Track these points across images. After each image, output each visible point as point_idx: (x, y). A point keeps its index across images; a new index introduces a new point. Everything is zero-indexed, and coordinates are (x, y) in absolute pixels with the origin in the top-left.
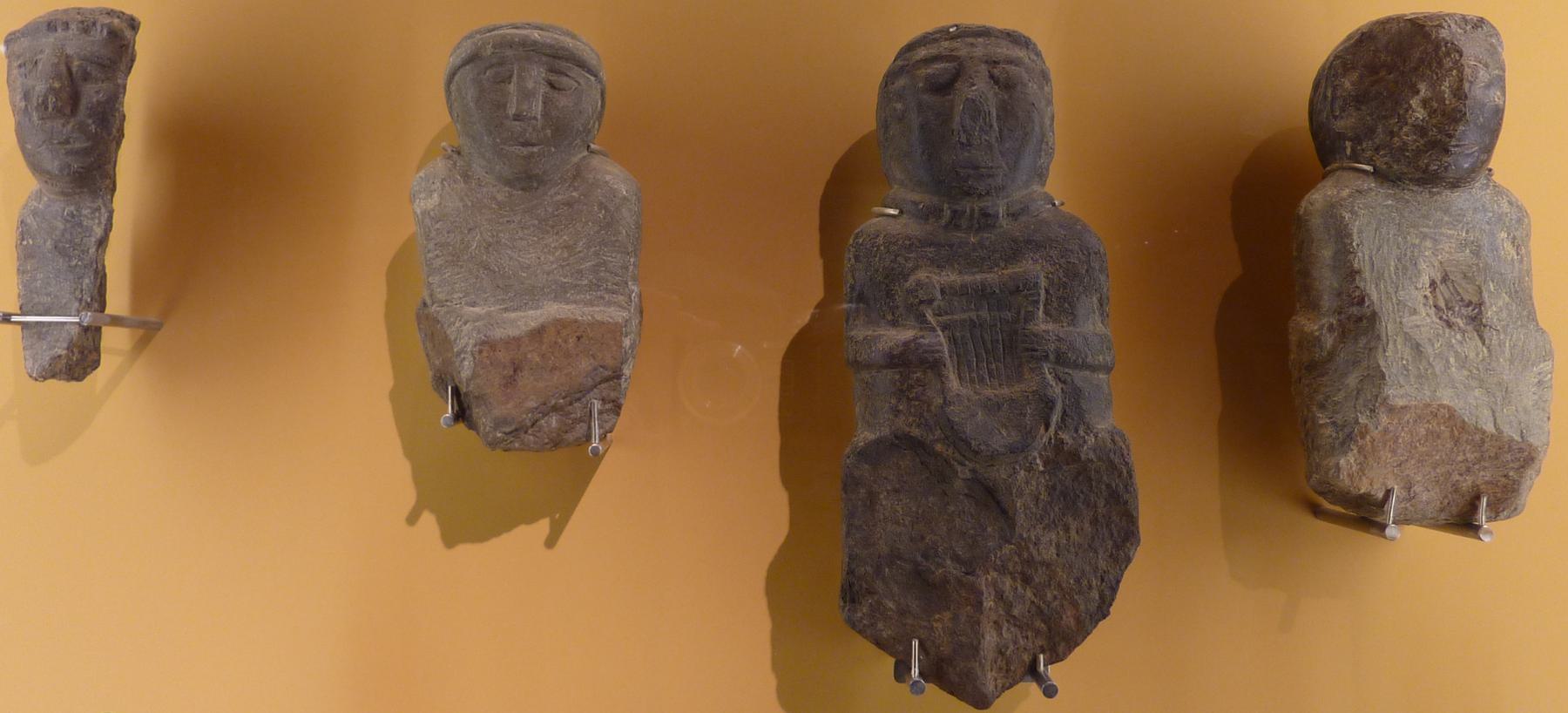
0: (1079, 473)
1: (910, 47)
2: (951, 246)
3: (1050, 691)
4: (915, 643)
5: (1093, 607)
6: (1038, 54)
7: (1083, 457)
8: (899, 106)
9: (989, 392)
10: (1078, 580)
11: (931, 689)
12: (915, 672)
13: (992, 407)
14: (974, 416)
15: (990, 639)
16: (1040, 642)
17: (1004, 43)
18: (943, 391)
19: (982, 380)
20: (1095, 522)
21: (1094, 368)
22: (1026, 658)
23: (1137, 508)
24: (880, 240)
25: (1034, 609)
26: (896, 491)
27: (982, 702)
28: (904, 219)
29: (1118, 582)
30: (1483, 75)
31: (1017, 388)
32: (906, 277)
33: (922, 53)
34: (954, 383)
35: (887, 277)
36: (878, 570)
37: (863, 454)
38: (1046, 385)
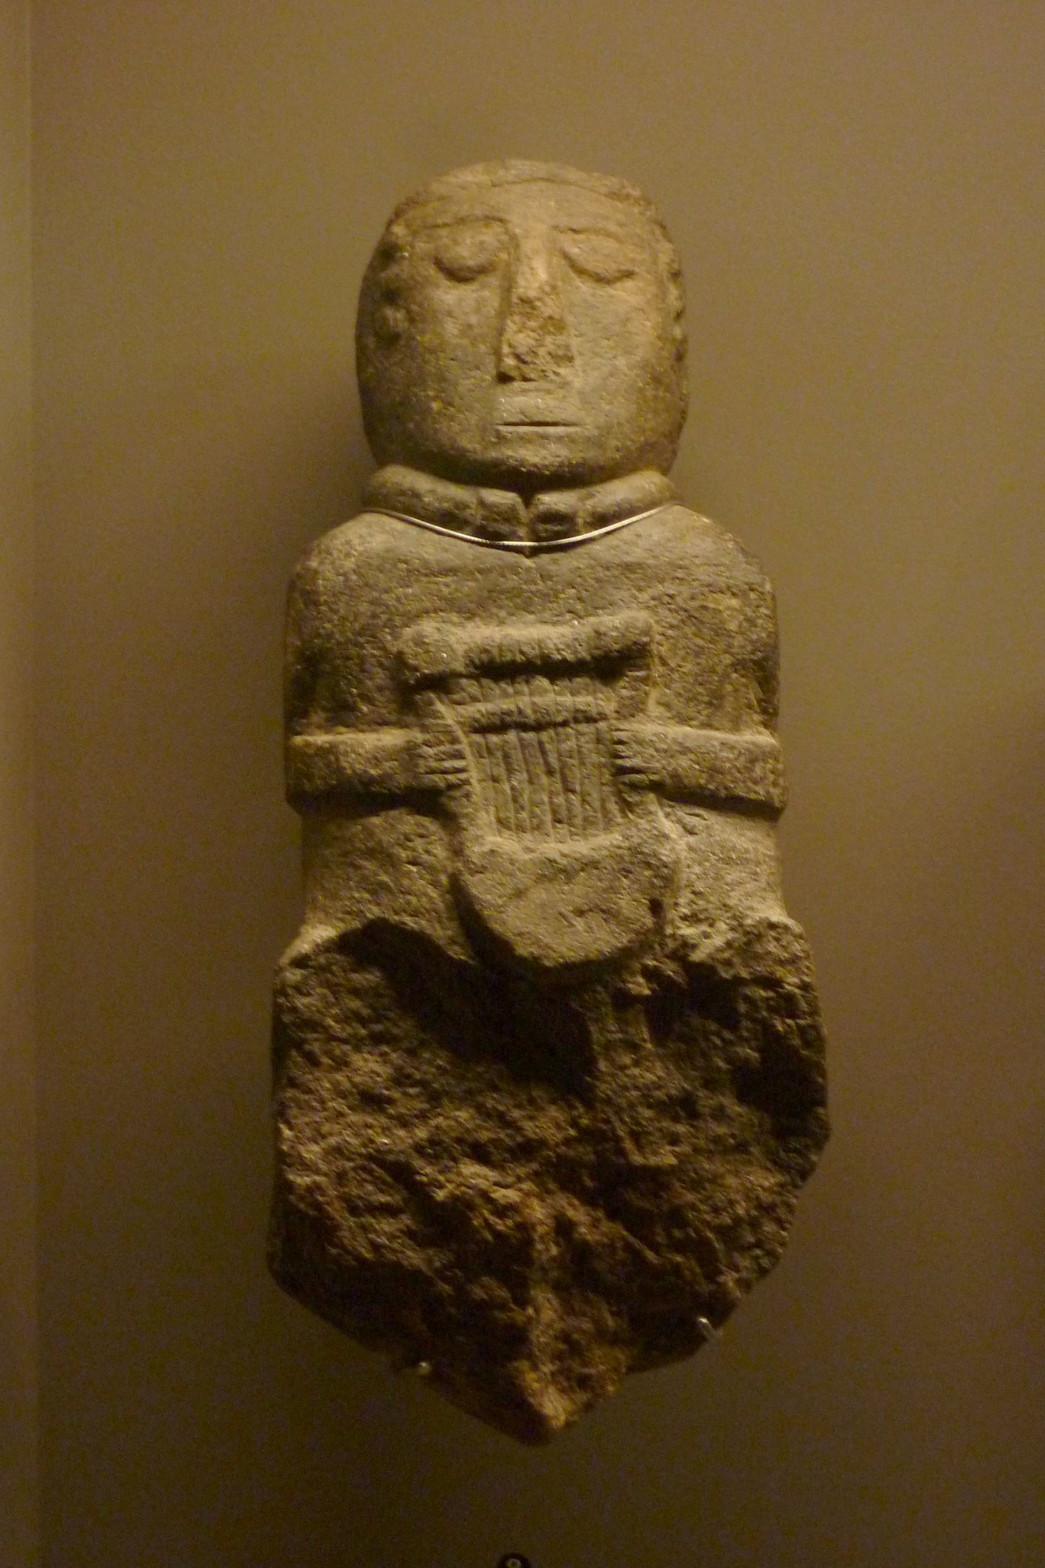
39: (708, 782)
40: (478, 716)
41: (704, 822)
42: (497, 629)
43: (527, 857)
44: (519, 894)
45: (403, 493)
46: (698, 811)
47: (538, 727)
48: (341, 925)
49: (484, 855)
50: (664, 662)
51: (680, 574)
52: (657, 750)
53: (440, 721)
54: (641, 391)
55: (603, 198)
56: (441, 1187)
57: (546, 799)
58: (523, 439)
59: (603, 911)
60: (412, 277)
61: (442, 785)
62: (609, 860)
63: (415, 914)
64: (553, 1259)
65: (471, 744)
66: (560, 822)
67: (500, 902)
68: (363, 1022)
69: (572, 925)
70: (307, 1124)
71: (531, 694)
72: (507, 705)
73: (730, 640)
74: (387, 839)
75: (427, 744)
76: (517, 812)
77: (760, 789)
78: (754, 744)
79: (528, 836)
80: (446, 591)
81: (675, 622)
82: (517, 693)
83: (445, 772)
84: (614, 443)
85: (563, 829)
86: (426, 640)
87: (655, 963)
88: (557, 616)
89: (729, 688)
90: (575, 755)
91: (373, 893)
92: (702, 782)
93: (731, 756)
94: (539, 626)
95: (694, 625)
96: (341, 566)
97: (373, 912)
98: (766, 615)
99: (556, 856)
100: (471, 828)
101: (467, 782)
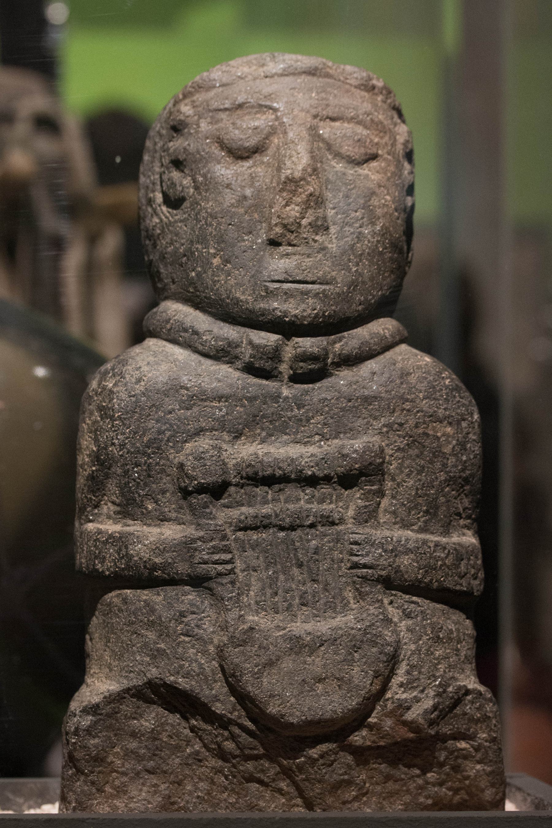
39: (424, 576)
42: (259, 447)
44: (270, 664)
45: (185, 330)
46: (414, 599)
47: (292, 528)
48: (125, 681)
49: (245, 632)
50: (393, 480)
51: (407, 406)
52: (385, 551)
54: (381, 254)
55: (353, 89)
58: (288, 295)
59: (338, 679)
60: (198, 152)
61: (213, 573)
63: (187, 675)
68: (140, 758)
72: (266, 510)
73: (445, 461)
74: (166, 615)
77: (464, 582)
78: (459, 544)
79: (279, 617)
84: (359, 298)
89: (442, 499)
91: (153, 657)
92: (420, 576)
93: (442, 555)
95: (417, 448)
96: (133, 389)
97: (153, 672)
98: (474, 440)
101: (232, 571)
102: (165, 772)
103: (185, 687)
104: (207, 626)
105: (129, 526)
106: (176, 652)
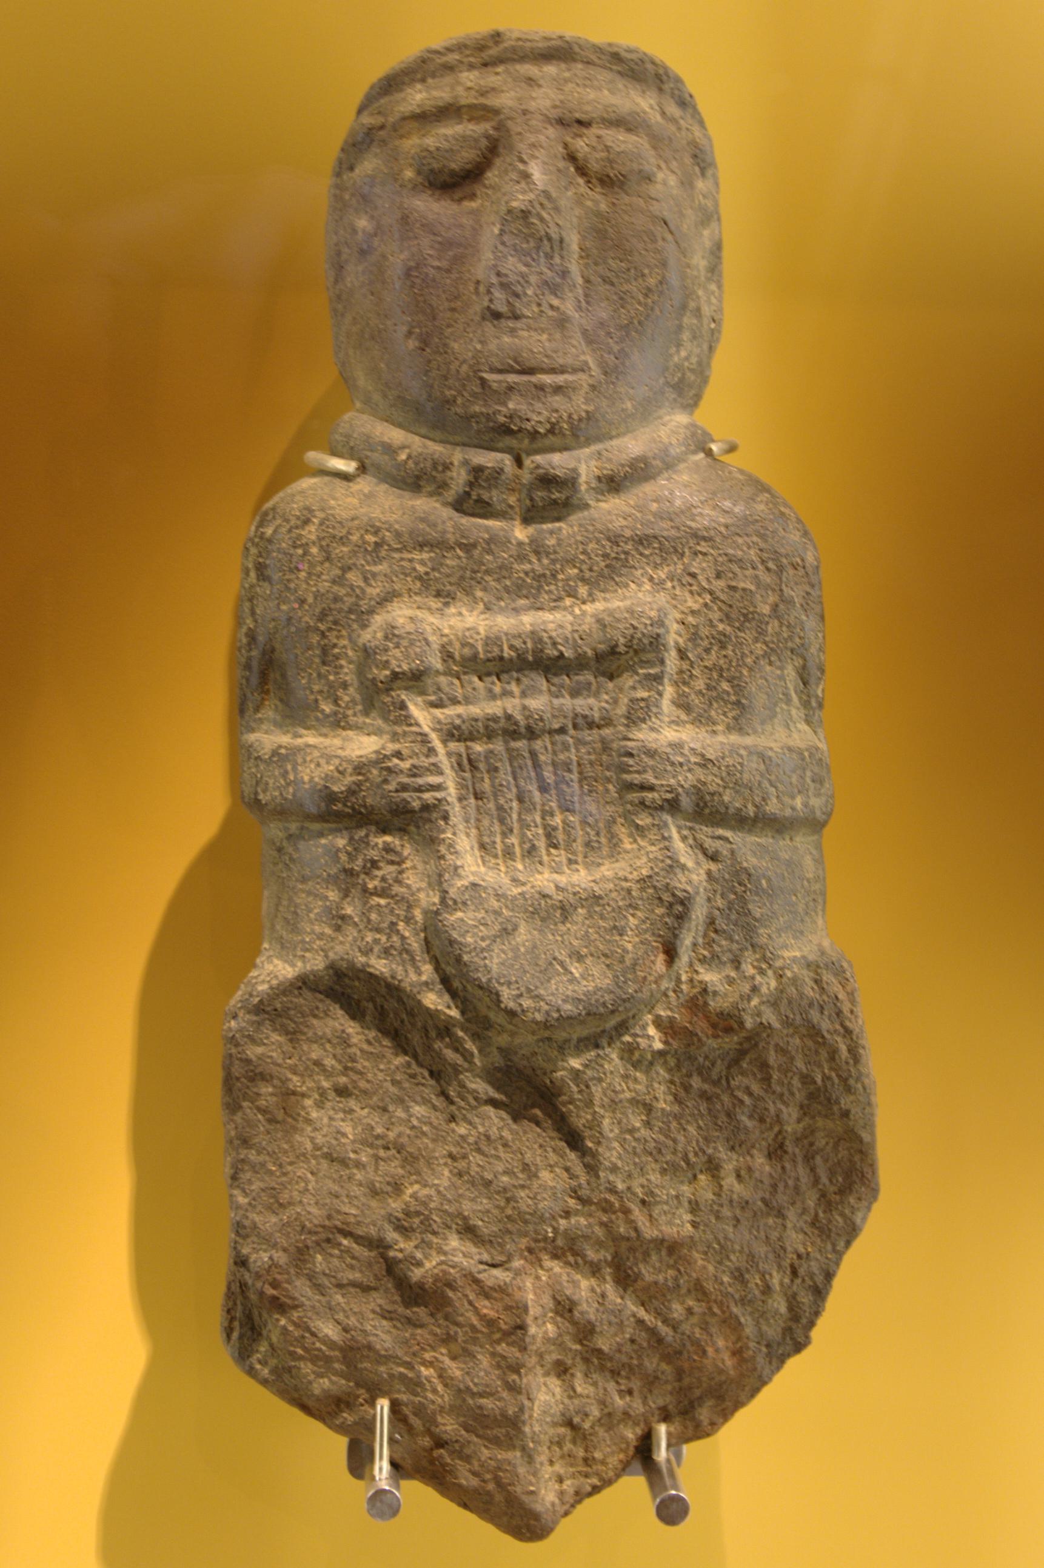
0: (742, 1053)
1: (391, 84)
2: (468, 548)
3: (672, 1511)
4: (383, 1405)
5: (772, 1331)
6: (685, 102)
7: (749, 1023)
8: (363, 223)
9: (544, 880)
10: (739, 1276)
11: (416, 1494)
12: (382, 1468)
13: (553, 911)
14: (507, 932)
15: (546, 1396)
16: (658, 1400)
17: (603, 76)
18: (438, 881)
19: (531, 851)
20: (776, 1152)
21: (778, 825)
22: (631, 1434)
23: (870, 1126)
24: (311, 532)
25: (642, 1337)
26: (342, 1092)
27: (525, 1524)
28: (364, 485)
29: (829, 1276)
30: (861, 1122)
31: (607, 870)
32: (363, 617)
33: (417, 97)
34: (470, 864)
35: (322, 616)
36: (301, 1255)
37: (271, 1010)
38: (674, 865)
40: (458, 722)
41: (729, 846)
43: (516, 891)
46: (720, 832)
53: (414, 729)
56: (419, 1264)
57: (538, 820)
59: (606, 956)
62: (614, 895)
64: (547, 1340)
65: (449, 754)
66: (556, 847)
67: (484, 944)
69: (567, 971)
70: (263, 1190)
71: (524, 694)
75: (398, 754)
76: (504, 835)
80: (421, 569)
81: (696, 607)
82: (506, 693)
83: (419, 789)
85: (561, 856)
86: (396, 632)
87: (669, 1013)
88: (555, 601)
90: (575, 768)
94: (532, 612)
99: (551, 889)
100: (449, 857)
102: (365, 1092)
103: (382, 973)
104: (412, 879)
105: (301, 737)
106: (369, 921)
